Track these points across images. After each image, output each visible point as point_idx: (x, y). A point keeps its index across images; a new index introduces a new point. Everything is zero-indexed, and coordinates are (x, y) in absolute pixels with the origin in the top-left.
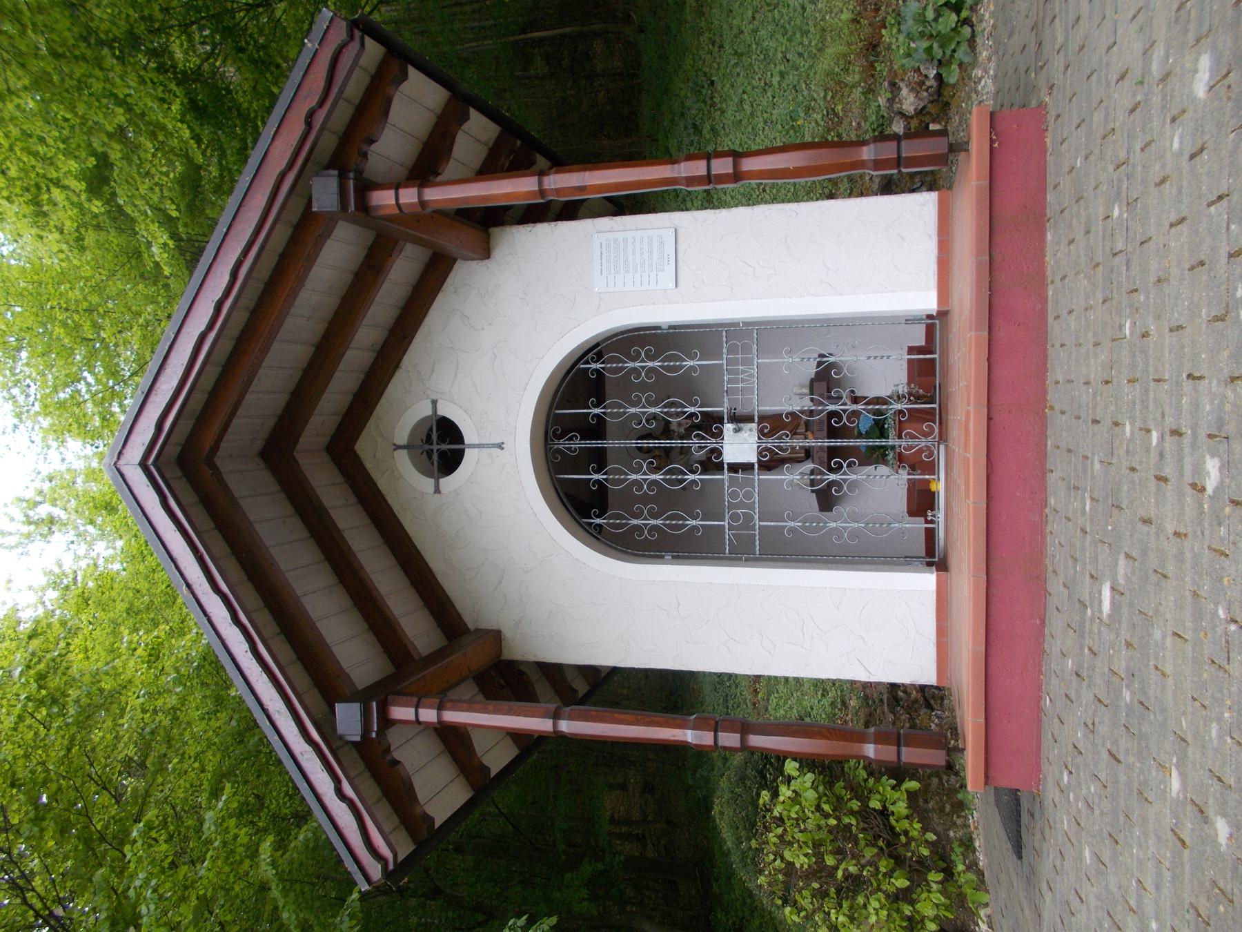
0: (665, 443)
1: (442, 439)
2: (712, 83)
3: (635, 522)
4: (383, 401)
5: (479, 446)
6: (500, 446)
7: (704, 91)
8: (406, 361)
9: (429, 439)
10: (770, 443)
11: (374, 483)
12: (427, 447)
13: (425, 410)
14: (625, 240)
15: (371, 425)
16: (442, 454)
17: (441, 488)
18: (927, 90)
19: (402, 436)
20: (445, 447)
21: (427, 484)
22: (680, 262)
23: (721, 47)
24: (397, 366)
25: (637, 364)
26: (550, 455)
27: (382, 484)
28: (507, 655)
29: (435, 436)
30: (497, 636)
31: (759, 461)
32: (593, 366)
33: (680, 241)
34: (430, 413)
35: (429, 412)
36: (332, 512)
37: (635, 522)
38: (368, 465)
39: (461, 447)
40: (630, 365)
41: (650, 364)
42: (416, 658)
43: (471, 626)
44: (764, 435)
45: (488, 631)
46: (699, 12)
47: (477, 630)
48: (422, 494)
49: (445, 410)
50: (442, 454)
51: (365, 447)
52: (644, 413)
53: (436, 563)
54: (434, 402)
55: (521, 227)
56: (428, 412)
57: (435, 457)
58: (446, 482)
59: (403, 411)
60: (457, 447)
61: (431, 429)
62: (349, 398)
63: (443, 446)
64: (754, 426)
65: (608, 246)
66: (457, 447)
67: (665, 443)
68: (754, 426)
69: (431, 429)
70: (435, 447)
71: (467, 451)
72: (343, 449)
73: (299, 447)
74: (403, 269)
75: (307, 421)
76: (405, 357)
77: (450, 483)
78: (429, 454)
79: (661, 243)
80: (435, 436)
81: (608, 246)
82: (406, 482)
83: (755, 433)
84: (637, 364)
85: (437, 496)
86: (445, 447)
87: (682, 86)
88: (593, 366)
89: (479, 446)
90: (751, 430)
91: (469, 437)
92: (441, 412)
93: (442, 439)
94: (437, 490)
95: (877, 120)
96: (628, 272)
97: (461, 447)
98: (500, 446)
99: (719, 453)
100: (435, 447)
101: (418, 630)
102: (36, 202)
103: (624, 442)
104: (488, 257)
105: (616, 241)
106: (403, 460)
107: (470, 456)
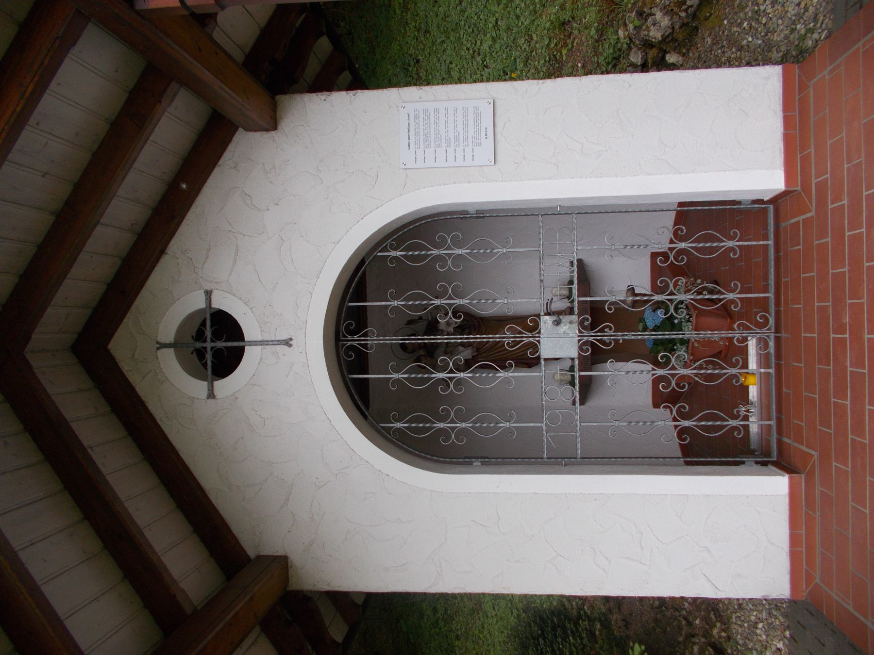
0: (428, 339)
1: (216, 337)
2: (418, 61)
3: (441, 425)
4: (144, 292)
5: (262, 343)
6: (288, 343)
7: (410, 69)
8: (174, 246)
9: (200, 335)
10: (526, 338)
11: (133, 389)
12: (199, 345)
13: (196, 302)
14: (436, 111)
15: (128, 320)
16: (217, 352)
17: (216, 392)
18: (686, 11)
19: (168, 331)
20: (220, 344)
21: (199, 387)
22: (498, 136)
23: (427, 32)
24: (163, 252)
25: (443, 252)
26: (342, 353)
27: (142, 388)
28: (294, 586)
29: (208, 333)
30: (282, 563)
31: (580, 357)
32: (393, 253)
33: (498, 113)
34: (203, 306)
35: (202, 305)
36: (74, 425)
37: (441, 425)
38: (125, 367)
39: (241, 344)
40: (435, 252)
41: (458, 251)
42: (189, 610)
43: (252, 553)
44: (585, 328)
45: (275, 559)
46: (405, 8)
47: (260, 558)
48: (193, 399)
49: (221, 302)
50: (217, 352)
51: (118, 346)
52: (450, 305)
53: (208, 480)
54: (208, 294)
55: (314, 95)
56: (200, 303)
57: (209, 357)
58: (220, 385)
59: (172, 301)
60: (235, 344)
61: (204, 324)
62: (101, 289)
63: (218, 344)
64: (574, 318)
65: (417, 117)
66: (235, 344)
67: (428, 339)
68: (574, 318)
69: (204, 324)
70: (209, 345)
71: (247, 349)
72: (93, 347)
73: (29, 347)
74: (172, 129)
75: (43, 310)
76: (173, 242)
77: (225, 386)
78: (200, 354)
79: (478, 115)
80: (208, 333)
81: (417, 117)
82: (175, 390)
83: (575, 326)
84: (443, 252)
85: (211, 401)
86: (220, 344)
87: (389, 67)
88: (393, 253)
89: (262, 343)
90: (571, 322)
91: (250, 333)
92: (217, 304)
93: (216, 337)
94: (211, 395)
95: (615, 52)
96: (439, 146)
97: (241, 344)
98: (288, 343)
99: (535, 347)
100: (209, 345)
101: (185, 566)
102: (480, 606)
103: (417, 341)
104: (275, 128)
105: (426, 111)
106: (169, 361)
107: (251, 355)
